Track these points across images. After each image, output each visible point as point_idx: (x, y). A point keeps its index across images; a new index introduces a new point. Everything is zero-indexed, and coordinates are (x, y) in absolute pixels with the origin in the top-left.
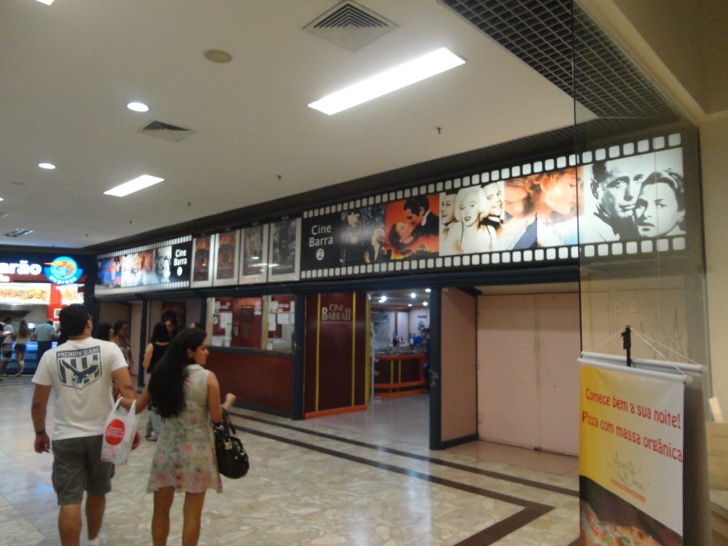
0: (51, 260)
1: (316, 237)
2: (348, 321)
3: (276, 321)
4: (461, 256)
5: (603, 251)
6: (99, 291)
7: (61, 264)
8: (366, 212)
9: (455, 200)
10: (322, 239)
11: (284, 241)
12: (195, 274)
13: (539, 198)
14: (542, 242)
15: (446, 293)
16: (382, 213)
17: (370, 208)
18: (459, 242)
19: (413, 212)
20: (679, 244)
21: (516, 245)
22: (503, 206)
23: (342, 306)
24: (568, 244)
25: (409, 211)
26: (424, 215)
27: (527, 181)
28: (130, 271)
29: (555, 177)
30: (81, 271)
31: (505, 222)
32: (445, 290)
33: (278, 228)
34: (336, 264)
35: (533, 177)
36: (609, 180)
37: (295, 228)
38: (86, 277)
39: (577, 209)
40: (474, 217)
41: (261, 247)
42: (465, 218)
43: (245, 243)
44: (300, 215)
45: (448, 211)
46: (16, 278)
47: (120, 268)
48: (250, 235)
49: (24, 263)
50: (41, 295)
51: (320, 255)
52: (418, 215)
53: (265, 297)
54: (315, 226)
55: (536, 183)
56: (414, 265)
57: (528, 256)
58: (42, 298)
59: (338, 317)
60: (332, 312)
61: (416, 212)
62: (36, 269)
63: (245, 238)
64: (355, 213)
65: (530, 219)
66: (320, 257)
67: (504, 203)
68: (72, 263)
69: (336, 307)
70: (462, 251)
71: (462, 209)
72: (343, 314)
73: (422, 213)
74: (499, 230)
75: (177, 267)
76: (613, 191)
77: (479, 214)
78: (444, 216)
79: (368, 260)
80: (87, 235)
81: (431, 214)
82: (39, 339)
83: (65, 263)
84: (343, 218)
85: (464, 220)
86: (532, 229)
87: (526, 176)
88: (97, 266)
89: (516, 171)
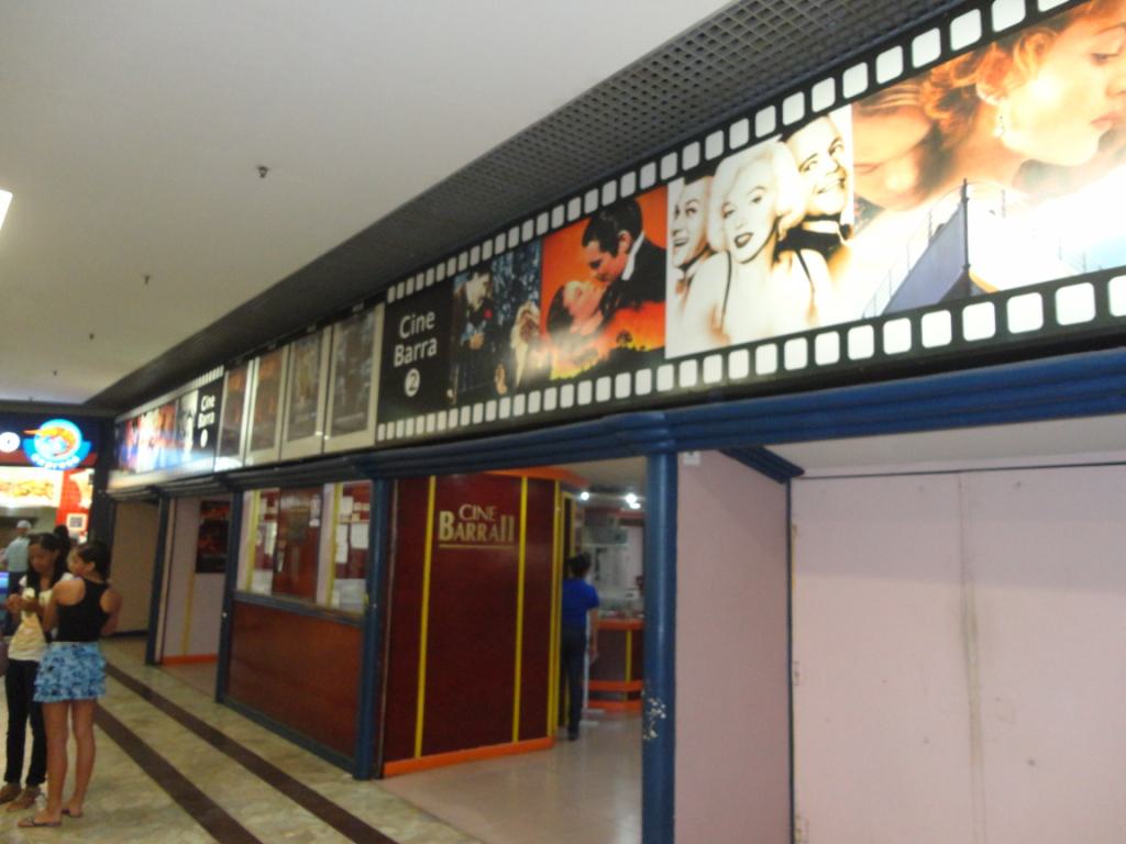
0: (37, 426)
1: (407, 343)
3: (349, 540)
4: (725, 352)
6: (120, 481)
7: (55, 433)
8: (501, 269)
9: (708, 194)
10: (417, 347)
11: (354, 360)
12: (223, 440)
13: (971, 131)
14: (987, 276)
15: (691, 468)
16: (536, 262)
17: (510, 256)
18: (719, 315)
19: (603, 248)
21: (893, 299)
22: (850, 182)
23: (491, 510)
24: (1092, 268)
25: (594, 245)
26: (628, 251)
27: (927, 86)
28: (147, 444)
29: (1030, 47)
31: (855, 229)
32: (689, 460)
33: (346, 332)
34: (443, 405)
35: (948, 66)
37: (373, 328)
38: (95, 456)
40: (761, 232)
41: (318, 376)
42: (736, 241)
43: (295, 369)
44: (382, 297)
47: (653, 260)
48: (302, 356)
50: (43, 489)
51: (412, 383)
52: (614, 253)
53: (329, 488)
54: (407, 318)
55: (962, 83)
57: (937, 332)
58: (45, 494)
59: (481, 534)
60: (465, 523)
61: (610, 245)
63: (295, 361)
64: (481, 273)
65: (942, 205)
66: (411, 389)
67: (850, 171)
68: (72, 431)
69: (477, 510)
70: (727, 337)
71: (726, 215)
72: (494, 528)
73: (623, 245)
74: (835, 259)
75: (202, 429)
77: (777, 220)
78: (678, 245)
79: (501, 388)
80: (55, 373)
81: (646, 245)
82: (10, 569)
83: (61, 431)
84: (457, 290)
85: (733, 247)
86: (951, 237)
88: (113, 435)
89: (889, 64)
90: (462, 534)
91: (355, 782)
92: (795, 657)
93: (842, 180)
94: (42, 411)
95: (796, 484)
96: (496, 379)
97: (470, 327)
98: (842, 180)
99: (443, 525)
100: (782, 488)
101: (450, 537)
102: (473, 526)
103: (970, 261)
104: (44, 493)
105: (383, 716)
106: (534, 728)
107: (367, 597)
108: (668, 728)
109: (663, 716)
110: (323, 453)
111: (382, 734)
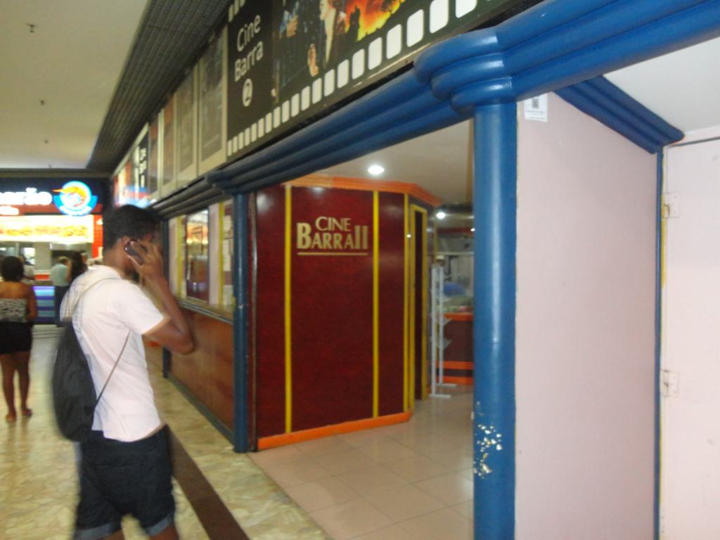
0: (60, 187)
2: (361, 250)
7: (73, 190)
10: (249, 56)
23: (345, 221)
30: (95, 198)
38: (101, 206)
46: (26, 211)
49: (31, 191)
59: (337, 243)
60: (321, 233)
62: (44, 198)
66: (247, 99)
69: (332, 221)
72: (349, 237)
80: (46, 142)
90: (319, 243)
91: (237, 454)
92: (664, 364)
94: (63, 176)
95: (670, 153)
96: (309, 61)
97: (286, 13)
99: (300, 235)
100: (653, 158)
101: (307, 246)
102: (329, 235)
104: (82, 234)
105: (254, 400)
106: (392, 404)
107: (234, 299)
108: (505, 463)
109: (499, 448)
110: (198, 177)
111: (254, 415)
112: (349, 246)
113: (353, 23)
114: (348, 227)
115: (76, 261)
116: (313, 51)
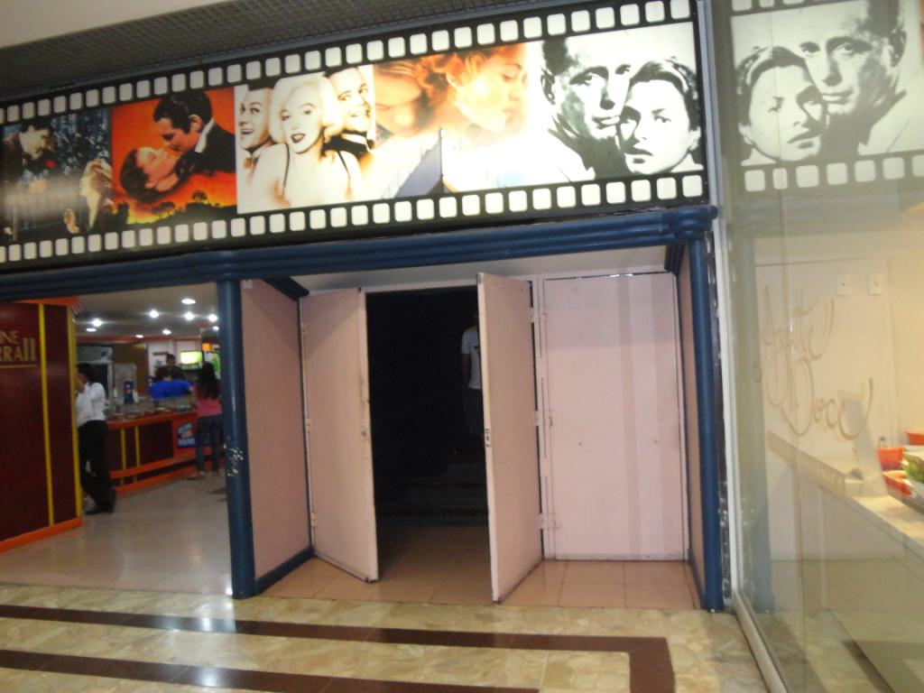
2: (30, 362)
4: (287, 213)
5: (566, 199)
14: (452, 183)
20: (693, 187)
36: (573, 71)
39: (513, 115)
40: (312, 136)
45: (256, 122)
56: (182, 234)
65: (427, 139)
72: (18, 349)
76: (579, 90)
81: (216, 129)
86: (431, 158)
87: (417, 58)
93: (368, 111)
98: (368, 111)
103: (444, 173)
112: (18, 359)
113: (184, 162)
114: (17, 340)
115: (157, 405)
116: (704, 592)
